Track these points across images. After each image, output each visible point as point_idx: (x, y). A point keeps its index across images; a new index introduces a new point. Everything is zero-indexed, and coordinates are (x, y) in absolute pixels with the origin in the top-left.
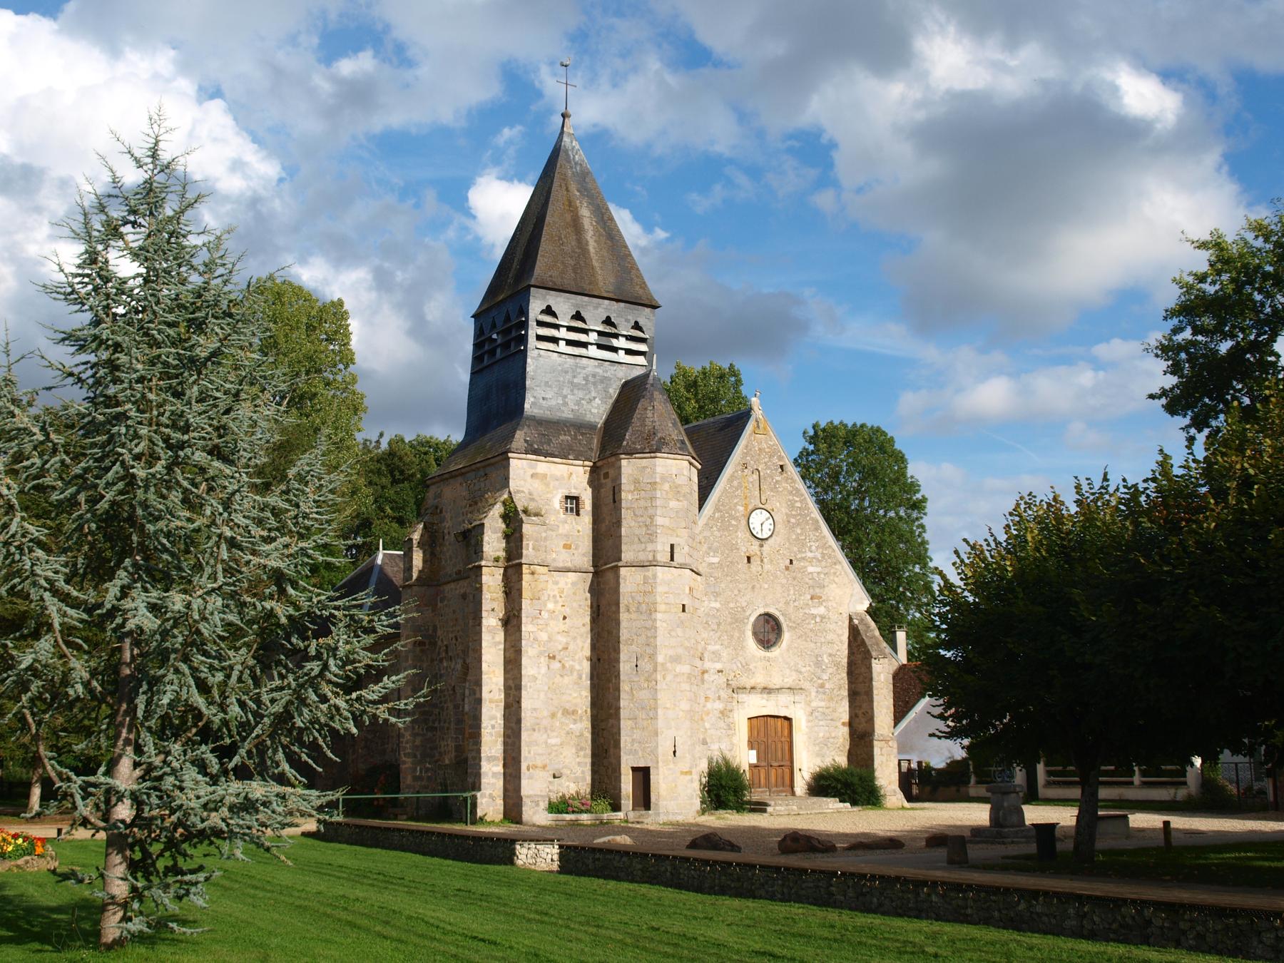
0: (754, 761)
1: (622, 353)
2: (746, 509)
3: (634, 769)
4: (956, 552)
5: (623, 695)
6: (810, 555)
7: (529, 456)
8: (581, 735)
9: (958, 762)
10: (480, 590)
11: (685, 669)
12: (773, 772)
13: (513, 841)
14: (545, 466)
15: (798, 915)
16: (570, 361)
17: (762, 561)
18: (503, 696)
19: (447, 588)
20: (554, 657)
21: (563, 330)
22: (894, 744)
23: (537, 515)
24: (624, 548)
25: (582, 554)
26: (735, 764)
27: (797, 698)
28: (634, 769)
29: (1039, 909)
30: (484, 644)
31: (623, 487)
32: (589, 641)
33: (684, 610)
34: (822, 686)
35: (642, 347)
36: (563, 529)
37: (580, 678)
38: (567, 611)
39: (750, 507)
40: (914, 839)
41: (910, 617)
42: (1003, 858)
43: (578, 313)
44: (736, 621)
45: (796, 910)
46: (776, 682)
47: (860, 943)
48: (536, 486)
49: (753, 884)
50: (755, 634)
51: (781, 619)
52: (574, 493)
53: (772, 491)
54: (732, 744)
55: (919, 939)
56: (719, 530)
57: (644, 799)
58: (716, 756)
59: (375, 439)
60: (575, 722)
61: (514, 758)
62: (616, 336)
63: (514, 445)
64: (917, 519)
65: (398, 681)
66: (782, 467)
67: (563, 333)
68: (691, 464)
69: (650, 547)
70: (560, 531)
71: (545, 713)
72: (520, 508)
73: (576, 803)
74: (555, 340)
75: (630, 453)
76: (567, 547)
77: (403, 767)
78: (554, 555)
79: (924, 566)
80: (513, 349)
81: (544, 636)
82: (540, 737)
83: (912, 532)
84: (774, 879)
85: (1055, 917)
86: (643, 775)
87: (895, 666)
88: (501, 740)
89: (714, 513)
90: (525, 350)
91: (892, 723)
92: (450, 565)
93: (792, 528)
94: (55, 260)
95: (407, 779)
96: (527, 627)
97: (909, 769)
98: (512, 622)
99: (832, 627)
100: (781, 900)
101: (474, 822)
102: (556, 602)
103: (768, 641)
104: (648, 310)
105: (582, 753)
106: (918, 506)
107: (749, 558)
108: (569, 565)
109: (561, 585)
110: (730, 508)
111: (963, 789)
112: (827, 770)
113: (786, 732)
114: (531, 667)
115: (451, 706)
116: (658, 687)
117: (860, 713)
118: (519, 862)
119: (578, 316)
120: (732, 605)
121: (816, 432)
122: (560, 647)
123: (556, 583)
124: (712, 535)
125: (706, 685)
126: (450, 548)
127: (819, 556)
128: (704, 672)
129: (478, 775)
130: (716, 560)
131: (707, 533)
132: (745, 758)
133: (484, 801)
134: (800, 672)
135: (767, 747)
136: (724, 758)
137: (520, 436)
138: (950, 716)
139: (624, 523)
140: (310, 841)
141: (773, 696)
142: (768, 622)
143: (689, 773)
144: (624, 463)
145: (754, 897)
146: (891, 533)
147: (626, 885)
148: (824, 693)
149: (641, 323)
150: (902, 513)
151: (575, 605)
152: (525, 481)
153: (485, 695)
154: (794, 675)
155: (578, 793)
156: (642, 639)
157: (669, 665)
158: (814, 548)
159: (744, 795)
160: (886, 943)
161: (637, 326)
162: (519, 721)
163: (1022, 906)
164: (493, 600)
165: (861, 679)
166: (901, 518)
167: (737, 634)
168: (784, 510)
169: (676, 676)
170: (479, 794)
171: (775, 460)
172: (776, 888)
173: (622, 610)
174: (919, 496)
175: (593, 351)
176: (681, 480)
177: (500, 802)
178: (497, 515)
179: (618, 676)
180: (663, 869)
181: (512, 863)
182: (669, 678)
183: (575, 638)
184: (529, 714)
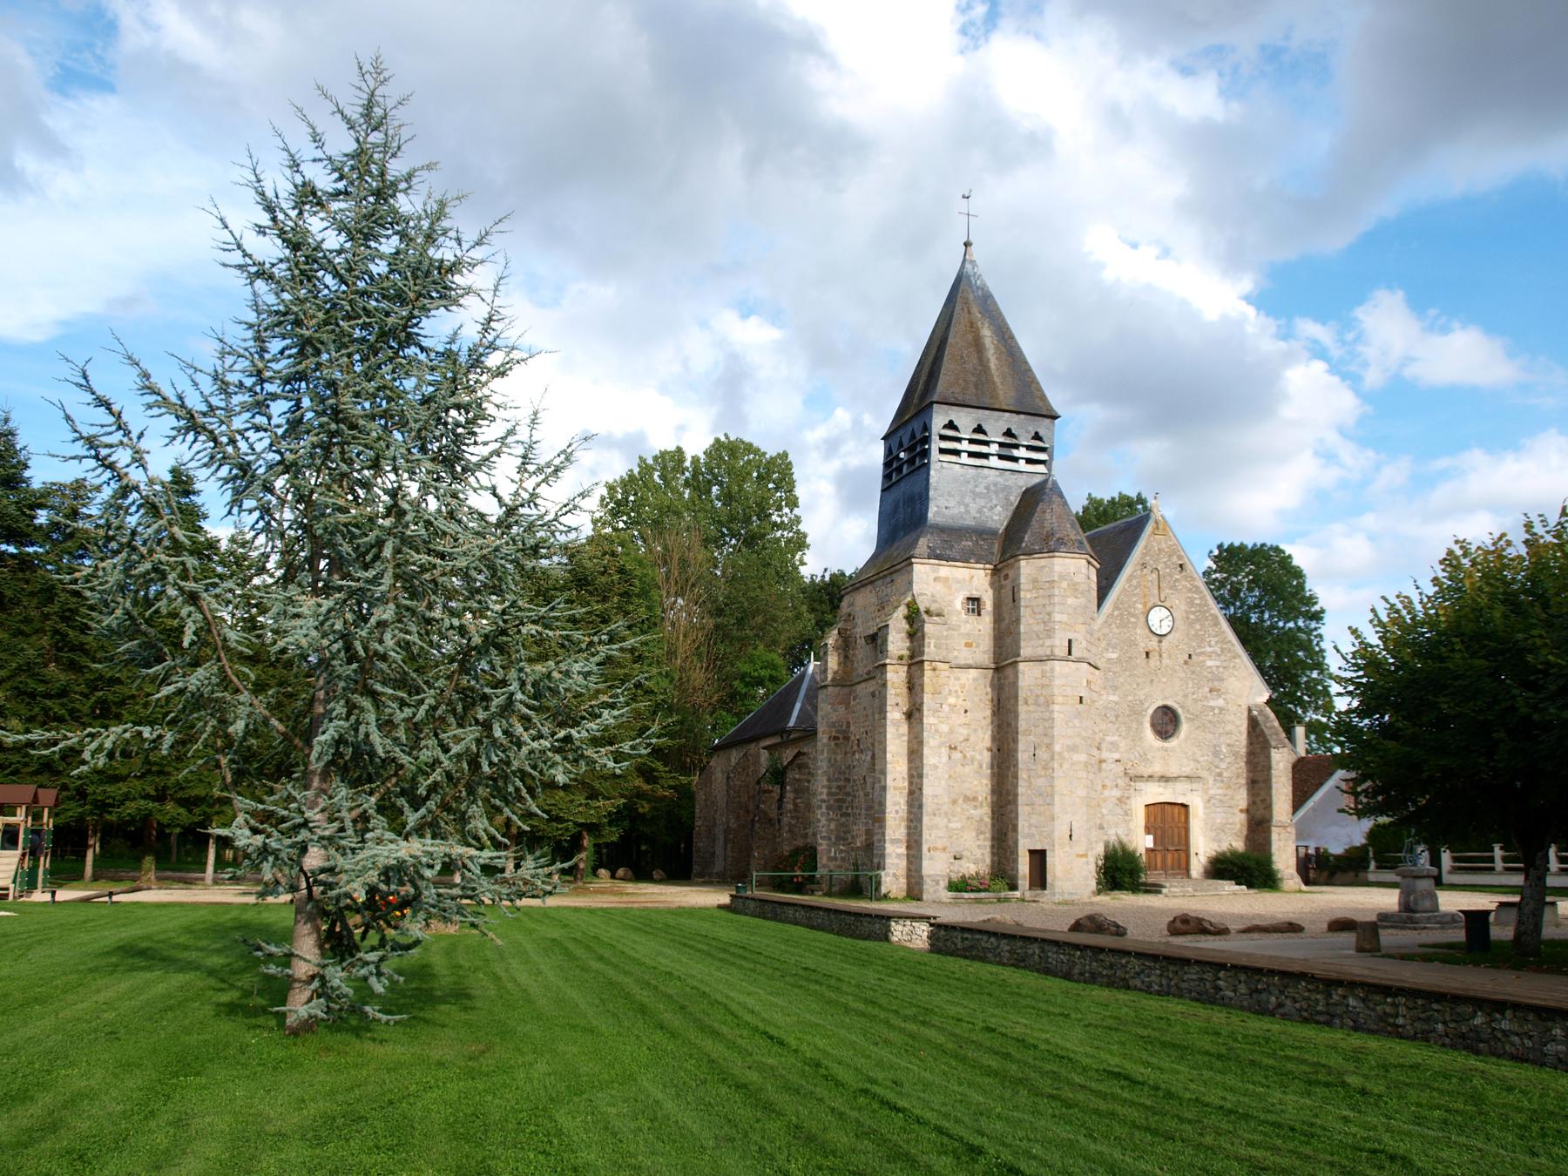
0: (1151, 845)
1: (1022, 462)
2: (1145, 606)
3: (1031, 852)
4: (1373, 610)
5: (1021, 783)
6: (1209, 649)
7: (932, 561)
8: (982, 820)
9: (1357, 848)
10: (884, 685)
11: (1082, 757)
12: (1169, 856)
13: (889, 918)
14: (946, 570)
15: (1174, 1014)
16: (972, 471)
18: (906, 784)
19: (859, 687)
20: (955, 748)
21: (965, 443)
22: (1293, 831)
23: (938, 615)
24: (1023, 644)
25: (983, 651)
26: (1131, 847)
27: (1195, 786)
28: (1031, 852)
29: (1505, 1025)
30: (888, 736)
31: (1022, 587)
32: (990, 732)
33: (1081, 702)
34: (1220, 775)
35: (1042, 456)
36: (965, 629)
37: (981, 767)
38: (968, 705)
39: (1150, 605)
40: (1313, 922)
41: (1307, 719)
42: (1421, 946)
43: (979, 426)
45: (1174, 1007)
46: (1174, 770)
47: (1253, 1063)
48: (939, 587)
49: (1127, 972)
50: (1153, 725)
51: (1180, 711)
52: (975, 594)
53: (1171, 588)
54: (1130, 830)
55: (1335, 1061)
57: (1039, 877)
58: (1113, 839)
59: (820, 574)
60: (975, 807)
61: (916, 841)
62: (1016, 446)
63: (917, 551)
64: (1316, 629)
65: (622, 715)
67: (965, 446)
68: (1089, 563)
69: (1048, 642)
70: (962, 630)
72: (922, 609)
73: (975, 883)
74: (957, 453)
75: (1029, 553)
76: (968, 645)
77: (819, 848)
78: (956, 653)
79: (1321, 672)
80: (918, 463)
81: (944, 728)
82: (941, 821)
83: (1310, 641)
84: (1150, 968)
85: (1530, 1037)
86: (1039, 857)
87: (1293, 758)
88: (904, 824)
90: (929, 463)
91: (1291, 810)
92: (862, 665)
93: (1192, 624)
94: (216, 213)
95: (822, 860)
96: (929, 719)
97: (1307, 855)
98: (914, 714)
99: (1231, 718)
100: (1159, 993)
101: (878, 899)
102: (958, 697)
103: (1166, 732)
104: (1047, 421)
105: (982, 837)
106: (1317, 616)
107: (1147, 654)
108: (970, 662)
109: (963, 680)
111: (1361, 875)
112: (1223, 854)
113: (1183, 818)
114: (933, 757)
115: (862, 794)
116: (1055, 775)
117: (1258, 800)
118: (894, 939)
119: (979, 429)
120: (1130, 698)
121: (1220, 553)
122: (961, 739)
123: (958, 679)
125: (1103, 774)
126: (861, 651)
128: (1101, 762)
129: (883, 856)
130: (1114, 656)
131: (1106, 631)
132: (1142, 842)
133: (888, 879)
135: (1164, 832)
136: (1121, 842)
137: (923, 544)
138: (1364, 791)
139: (1023, 620)
140: (723, 912)
141: (1170, 784)
142: (1166, 714)
143: (1085, 856)
144: (1023, 563)
145: (1128, 988)
146: (1289, 643)
147: (989, 967)
149: (1041, 434)
150: (1301, 623)
151: (976, 699)
152: (928, 584)
153: (889, 782)
154: (1192, 765)
155: (977, 874)
156: (1040, 730)
157: (1066, 754)
159: (1139, 877)
160: (1290, 1066)
161: (1037, 437)
162: (921, 807)
163: (1478, 1020)
164: (896, 695)
165: (1259, 768)
166: (1299, 629)
167: (1134, 725)
168: (1183, 607)
169: (1072, 764)
170: (883, 873)
171: (1175, 559)
172: (1153, 978)
173: (1021, 701)
174: (1317, 608)
175: (994, 462)
176: (1080, 578)
177: (903, 881)
178: (901, 616)
179: (1016, 766)
180: (1030, 952)
181: (887, 939)
182: (1066, 766)
183: (975, 730)
184: (930, 800)
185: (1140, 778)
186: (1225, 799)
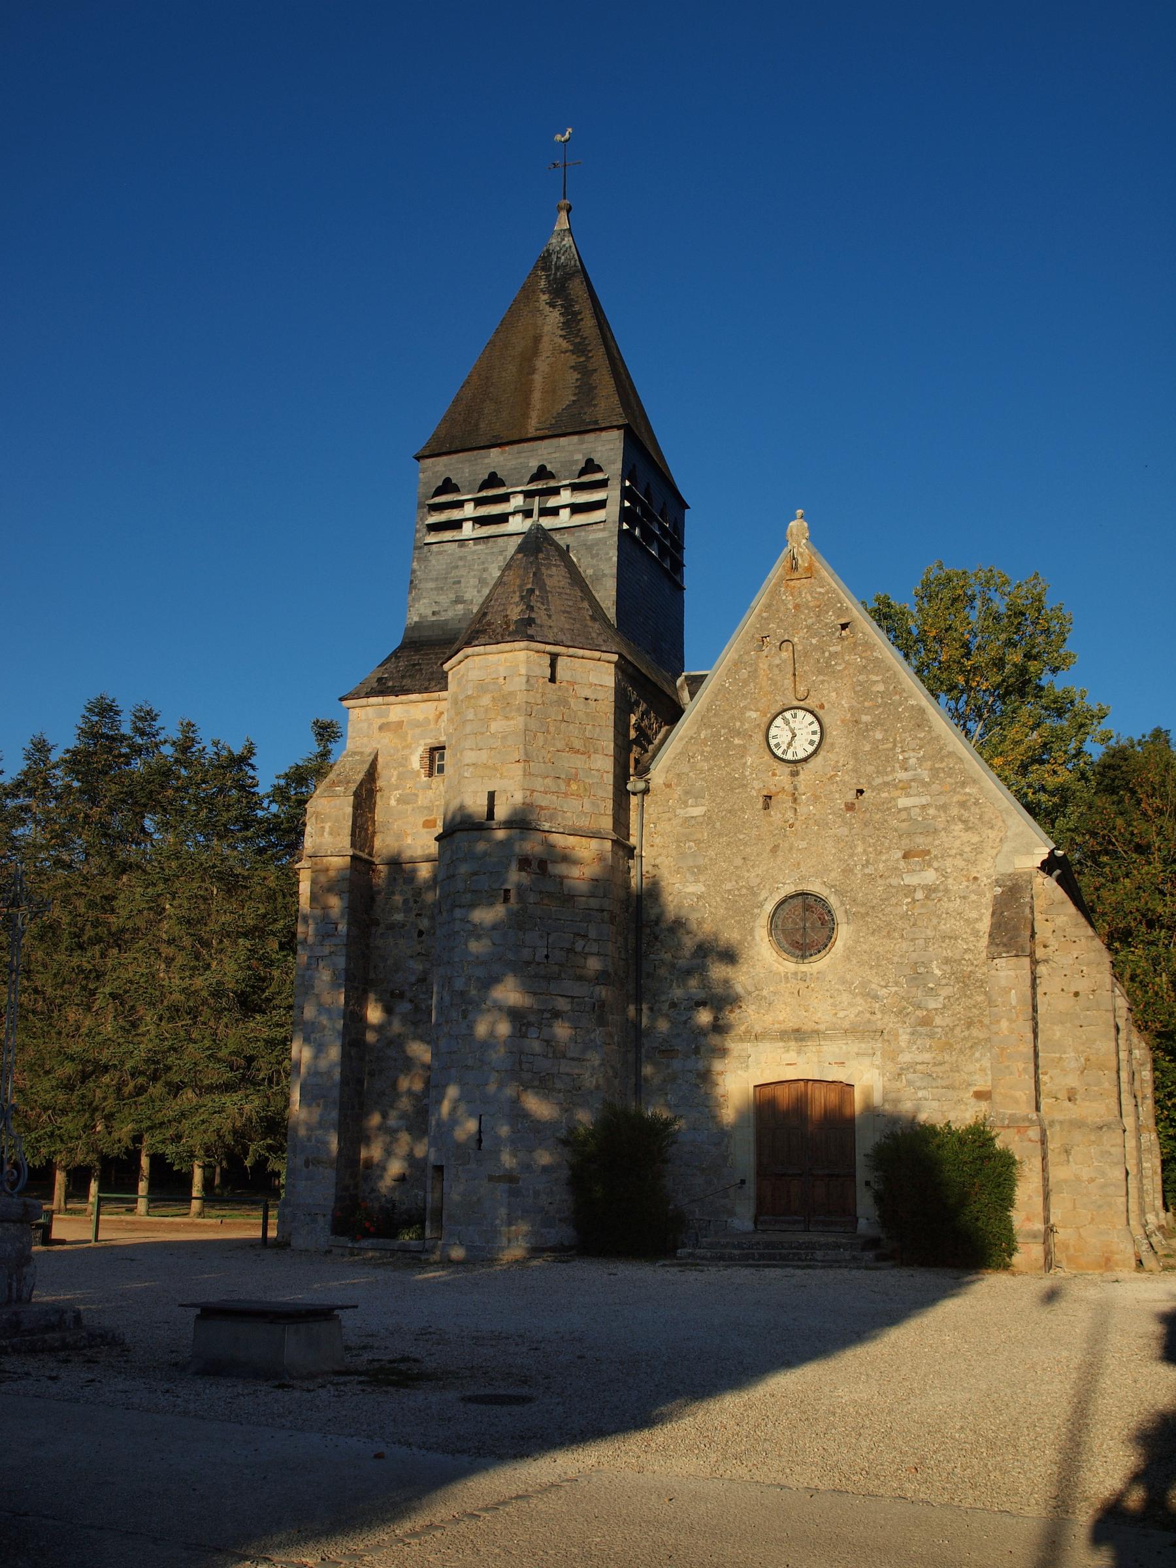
6: (901, 775)
51: (833, 901)
56: (706, 759)
89: (698, 732)
120: (729, 886)
127: (926, 776)
130: (697, 811)
134: (876, 997)
148: (931, 1036)
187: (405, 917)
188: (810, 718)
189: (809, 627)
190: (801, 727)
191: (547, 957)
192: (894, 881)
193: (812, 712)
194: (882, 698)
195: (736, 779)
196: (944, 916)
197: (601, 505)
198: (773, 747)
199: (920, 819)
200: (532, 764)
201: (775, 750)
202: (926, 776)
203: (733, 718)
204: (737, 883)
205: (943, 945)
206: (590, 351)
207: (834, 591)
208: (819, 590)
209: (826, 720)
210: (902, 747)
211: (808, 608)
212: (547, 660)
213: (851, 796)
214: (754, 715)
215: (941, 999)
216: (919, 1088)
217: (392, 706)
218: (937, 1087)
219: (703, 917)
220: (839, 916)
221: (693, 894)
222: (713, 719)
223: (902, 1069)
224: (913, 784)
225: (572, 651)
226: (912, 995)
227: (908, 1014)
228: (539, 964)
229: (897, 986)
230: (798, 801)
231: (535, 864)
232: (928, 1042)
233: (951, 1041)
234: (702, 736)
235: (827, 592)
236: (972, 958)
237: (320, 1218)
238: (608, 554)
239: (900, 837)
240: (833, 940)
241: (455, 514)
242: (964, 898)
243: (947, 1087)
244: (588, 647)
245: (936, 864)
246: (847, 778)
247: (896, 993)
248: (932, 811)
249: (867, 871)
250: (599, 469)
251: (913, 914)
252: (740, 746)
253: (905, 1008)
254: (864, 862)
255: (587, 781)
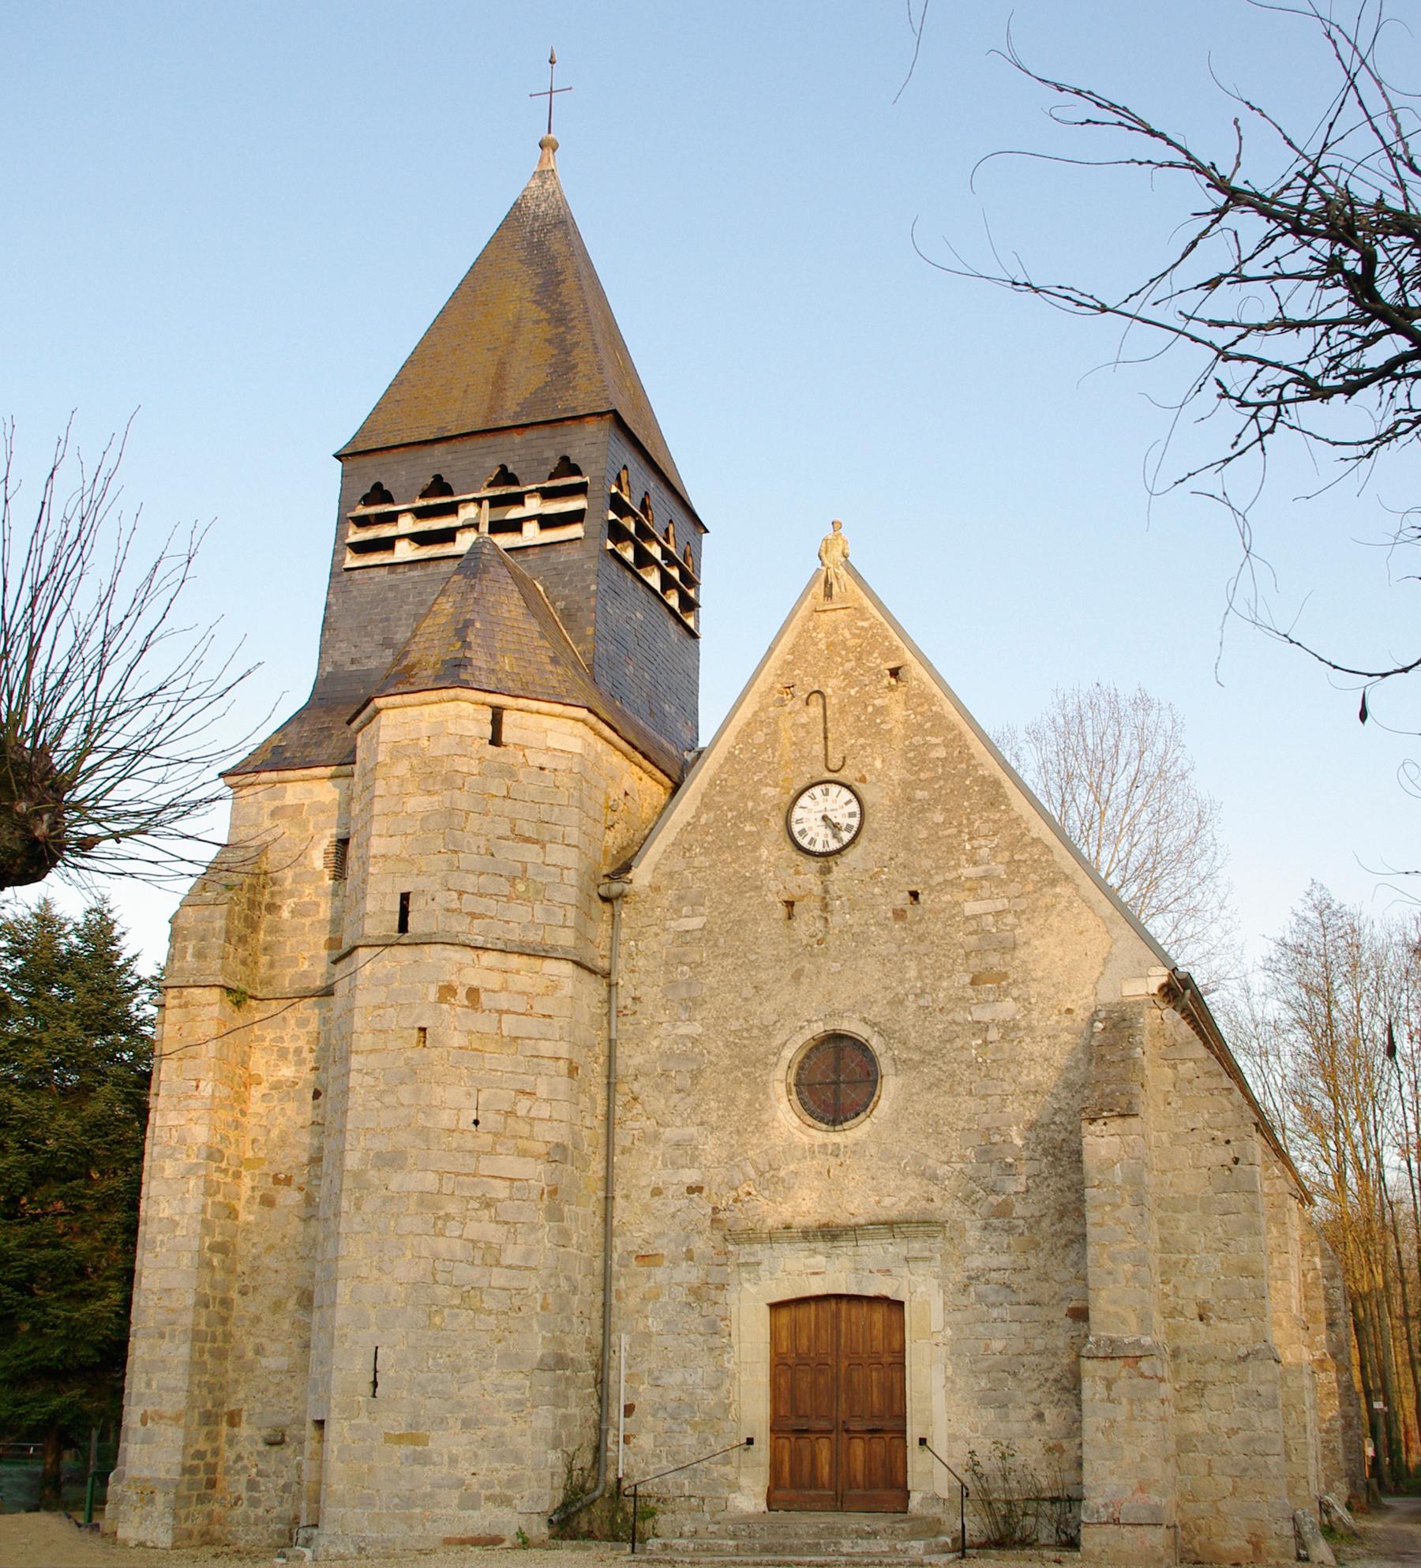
6: (968, 871)
17: (825, 907)
44: (745, 1062)
46: (857, 1206)
51: (876, 1043)
54: (722, 1372)
56: (707, 852)
66: (894, 673)
71: (190, 1300)
89: (697, 816)
107: (790, 904)
110: (743, 796)
120: (735, 1025)
124: (689, 866)
127: (1001, 871)
130: (695, 923)
134: (934, 1178)
141: (846, 1247)
148: (1011, 1229)
157: (372, 1174)
158: (985, 852)
167: (744, 1094)
169: (388, 1200)
182: (368, 1207)
185: (751, 1236)
186: (1018, 1279)
187: (297, 1071)
188: (846, 795)
189: (846, 675)
190: (835, 806)
191: (476, 1122)
192: (959, 1016)
193: (849, 788)
194: (943, 766)
195: (747, 879)
196: (1026, 1063)
197: (576, 517)
198: (796, 835)
199: (994, 930)
200: (461, 855)
201: (799, 839)
202: (1001, 871)
203: (743, 796)
204: (747, 1021)
205: (1025, 1103)
206: (572, 320)
207: (881, 624)
208: (860, 624)
209: (867, 798)
210: (969, 833)
211: (845, 648)
212: (488, 714)
213: (902, 899)
214: (770, 792)
215: (1023, 1178)
216: (993, 1305)
217: (288, 785)
218: (1019, 1304)
219: (699, 1069)
220: (885, 1064)
221: (688, 1036)
222: (717, 799)
223: (970, 1278)
224: (984, 882)
225: (522, 703)
226: (982, 1174)
227: (977, 1201)
228: (463, 1132)
229: (963, 1161)
230: (830, 908)
231: (462, 993)
232: (1005, 1239)
233: (1037, 1238)
234: (703, 821)
235: (871, 628)
236: (1065, 1122)
237: (160, 1498)
238: (584, 581)
239: (967, 955)
240: (875, 1098)
241: (386, 531)
242: (1055, 1037)
243: (1032, 1303)
244: (545, 698)
245: (1015, 992)
246: (896, 876)
247: (962, 1171)
248: (1010, 919)
249: (922, 1002)
250: (576, 471)
251: (985, 1061)
252: (751, 834)
253: (973, 1192)
254: (919, 991)
255: (538, 879)
